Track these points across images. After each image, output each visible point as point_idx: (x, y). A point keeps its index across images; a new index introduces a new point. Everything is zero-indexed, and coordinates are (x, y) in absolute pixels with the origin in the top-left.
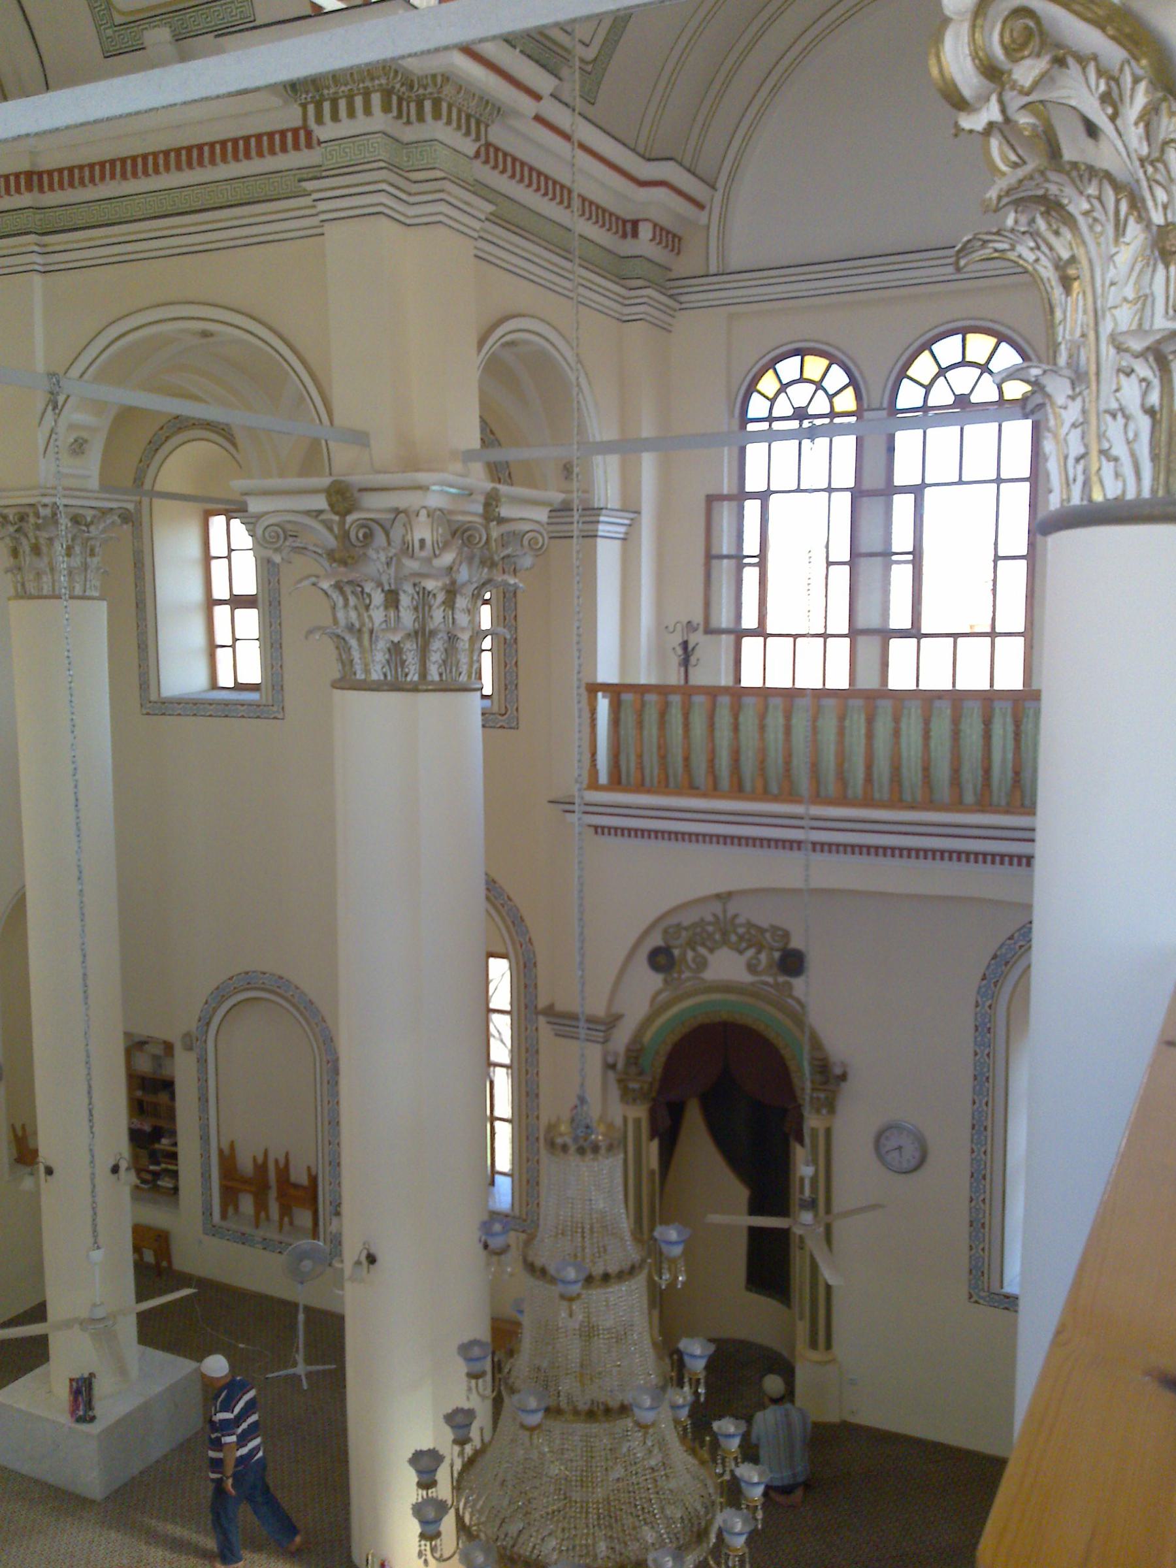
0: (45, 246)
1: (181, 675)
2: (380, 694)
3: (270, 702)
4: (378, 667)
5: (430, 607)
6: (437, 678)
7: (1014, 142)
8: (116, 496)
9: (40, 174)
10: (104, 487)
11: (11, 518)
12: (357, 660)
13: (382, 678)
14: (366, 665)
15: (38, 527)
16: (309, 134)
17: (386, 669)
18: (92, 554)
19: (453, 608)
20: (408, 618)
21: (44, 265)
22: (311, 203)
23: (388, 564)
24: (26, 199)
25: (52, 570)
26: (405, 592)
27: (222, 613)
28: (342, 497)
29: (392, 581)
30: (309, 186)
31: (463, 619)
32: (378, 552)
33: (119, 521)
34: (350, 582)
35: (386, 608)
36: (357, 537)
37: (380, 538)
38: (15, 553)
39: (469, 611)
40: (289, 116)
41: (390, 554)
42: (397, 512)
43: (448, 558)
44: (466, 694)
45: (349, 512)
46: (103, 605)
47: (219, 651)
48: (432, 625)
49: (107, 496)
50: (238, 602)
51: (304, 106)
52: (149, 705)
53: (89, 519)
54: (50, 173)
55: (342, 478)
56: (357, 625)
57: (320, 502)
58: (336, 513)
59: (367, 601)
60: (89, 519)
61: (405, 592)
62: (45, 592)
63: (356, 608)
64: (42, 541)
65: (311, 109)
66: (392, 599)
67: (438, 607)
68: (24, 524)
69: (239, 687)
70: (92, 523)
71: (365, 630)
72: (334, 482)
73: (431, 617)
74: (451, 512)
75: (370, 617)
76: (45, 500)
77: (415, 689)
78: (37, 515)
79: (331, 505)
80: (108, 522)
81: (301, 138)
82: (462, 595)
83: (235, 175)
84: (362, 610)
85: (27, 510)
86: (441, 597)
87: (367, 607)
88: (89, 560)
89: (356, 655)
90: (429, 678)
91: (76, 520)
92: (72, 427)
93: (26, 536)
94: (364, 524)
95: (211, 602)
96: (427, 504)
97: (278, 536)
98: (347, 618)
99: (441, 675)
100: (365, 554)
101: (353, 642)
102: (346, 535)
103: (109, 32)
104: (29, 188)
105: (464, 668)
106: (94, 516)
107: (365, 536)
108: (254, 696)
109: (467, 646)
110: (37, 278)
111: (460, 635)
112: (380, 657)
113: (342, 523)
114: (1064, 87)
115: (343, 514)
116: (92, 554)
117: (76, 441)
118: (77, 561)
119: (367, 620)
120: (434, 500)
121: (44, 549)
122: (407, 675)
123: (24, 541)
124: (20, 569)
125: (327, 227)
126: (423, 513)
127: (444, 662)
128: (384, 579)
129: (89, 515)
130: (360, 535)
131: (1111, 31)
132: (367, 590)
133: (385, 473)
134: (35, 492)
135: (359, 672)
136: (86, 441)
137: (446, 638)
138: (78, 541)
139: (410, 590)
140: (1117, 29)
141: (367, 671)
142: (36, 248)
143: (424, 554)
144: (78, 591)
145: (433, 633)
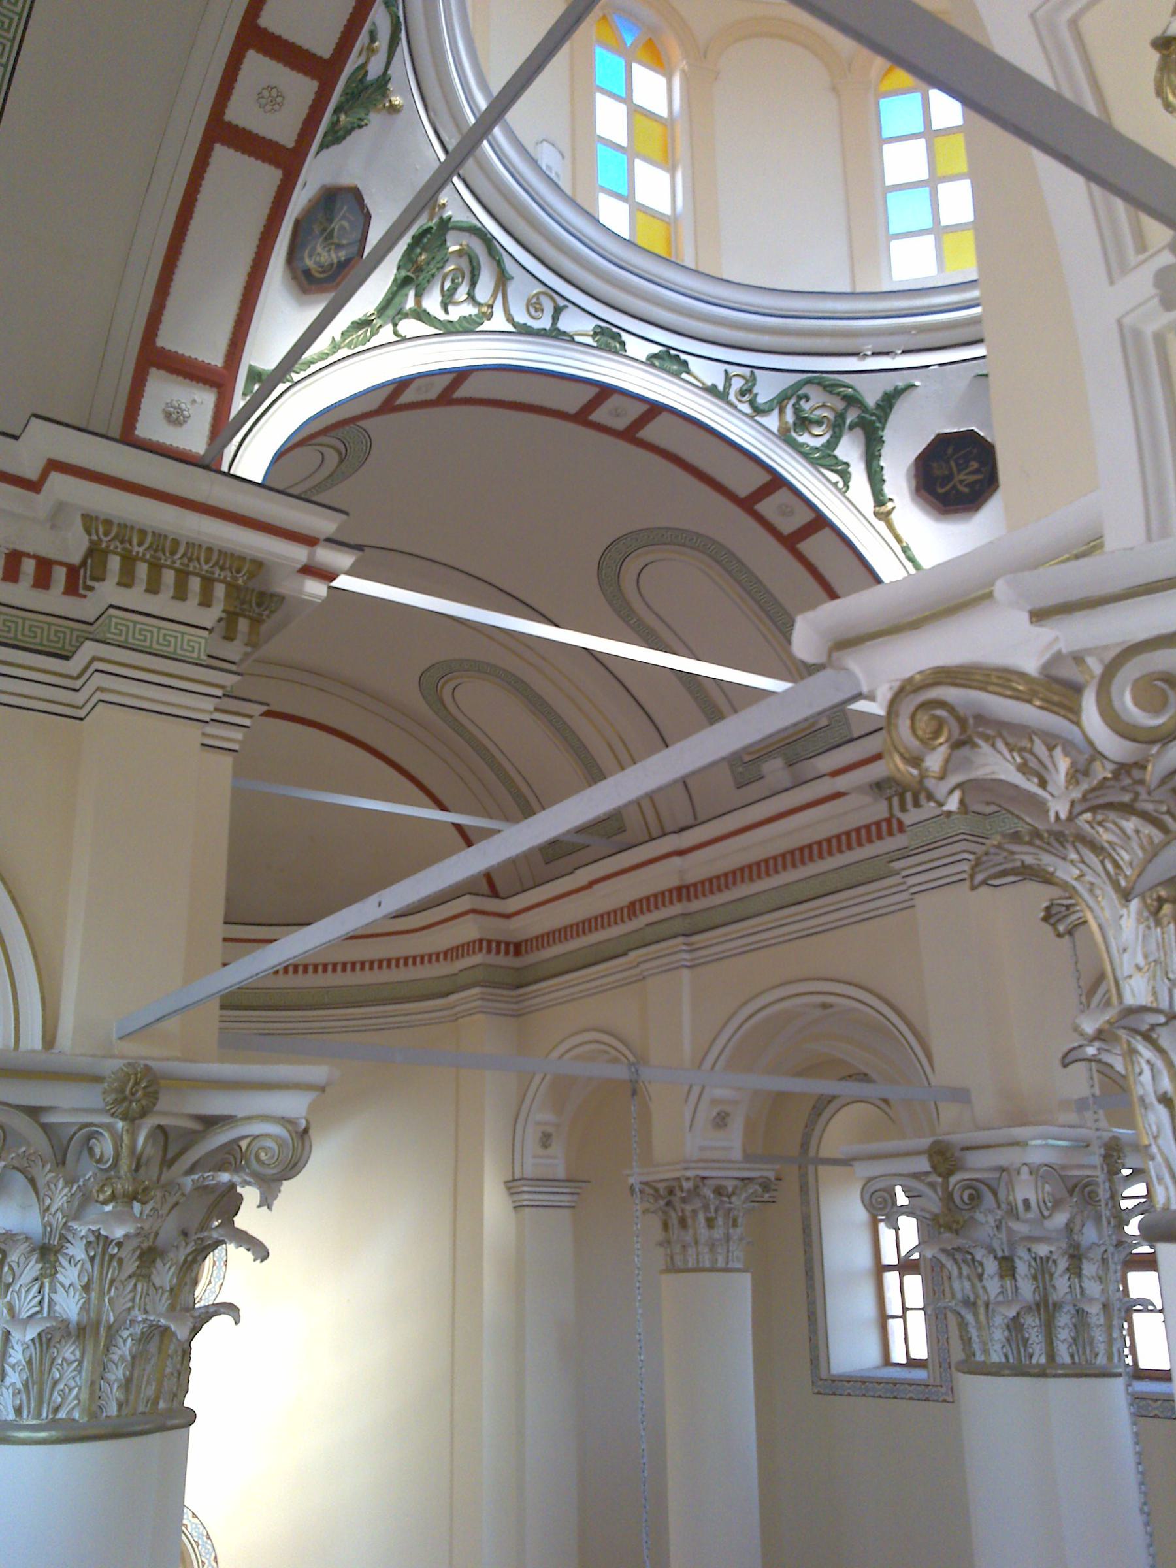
0: (692, 944)
1: (852, 1351)
2: (1001, 1379)
3: (938, 1382)
4: (998, 1347)
5: (1051, 1275)
6: (1068, 1360)
7: (1016, 812)
8: (757, 1166)
9: (687, 887)
10: (748, 1157)
11: (662, 1192)
12: (975, 1338)
13: (1003, 1360)
14: (984, 1344)
15: (684, 1200)
16: (900, 823)
17: (1007, 1349)
18: (735, 1225)
19: (1079, 1275)
20: (1027, 1289)
21: (692, 960)
22: (902, 881)
23: (998, 1227)
24: (677, 909)
25: (696, 1243)
26: (1020, 1258)
27: (891, 1278)
28: (944, 1159)
29: (1005, 1247)
30: (897, 865)
31: (1093, 1288)
32: (986, 1216)
33: (760, 1190)
34: (958, 1249)
35: (1002, 1277)
36: (962, 1200)
37: (988, 1199)
38: (666, 1226)
39: (1100, 1278)
40: (878, 810)
41: (998, 1217)
42: (1002, 1169)
43: (1060, 1219)
44: (1107, 1380)
45: (950, 1173)
46: (747, 1277)
47: (891, 1322)
48: (1054, 1297)
49: (748, 1165)
50: (905, 1266)
51: (889, 799)
52: (820, 1383)
53: (730, 1190)
54: (695, 885)
55: (946, 1138)
56: (972, 1298)
57: (923, 1164)
58: (940, 1175)
59: (980, 1270)
60: (730, 1190)
61: (1020, 1258)
62: (690, 1265)
63: (969, 1278)
64: (688, 1213)
65: (896, 800)
66: (1007, 1267)
67: (1061, 1276)
68: (672, 1198)
69: (912, 1363)
70: (734, 1193)
71: (980, 1303)
72: (935, 1143)
73: (1054, 1287)
74: (1064, 1167)
75: (984, 1288)
76: (689, 1174)
77: (1042, 1373)
78: (682, 1190)
79: (934, 1167)
80: (751, 1191)
81: (890, 826)
82: (1090, 1260)
83: (841, 864)
84: (976, 1281)
85: (675, 1184)
86: (1063, 1263)
87: (980, 1277)
88: (731, 1231)
89: (974, 1333)
90: (1059, 1360)
91: (719, 1191)
92: (714, 1102)
93: (675, 1210)
94: (970, 1185)
95: (881, 1269)
96: (1029, 1161)
97: (885, 1200)
98: (962, 1290)
99: (1072, 1356)
100: (972, 1218)
101: (969, 1318)
102: (950, 1196)
103: (740, 769)
104: (680, 900)
105: (1101, 1348)
106: (736, 1187)
107: (971, 1197)
108: (920, 1374)
109: (1102, 1321)
110: (685, 972)
111: (1086, 1308)
112: (999, 1335)
113: (946, 1184)
114: (984, 765)
115: (947, 1175)
116: (735, 1225)
117: (719, 1114)
118: (718, 1233)
119: (981, 1291)
120: (1037, 1155)
121: (689, 1221)
122: (1031, 1356)
123: (673, 1214)
124: (669, 1242)
125: (919, 900)
126: (1025, 1170)
127: (1074, 1339)
128: (996, 1244)
129: (730, 1185)
130: (966, 1197)
131: (1038, 703)
132: (978, 1257)
133: (989, 1129)
134: (678, 1167)
135: (978, 1354)
136: (727, 1114)
137: (1073, 1312)
138: (720, 1213)
139: (1026, 1257)
140: (1042, 700)
141: (986, 1352)
142: (684, 948)
143: (1030, 1215)
144: (721, 1263)
145: (1057, 1306)
